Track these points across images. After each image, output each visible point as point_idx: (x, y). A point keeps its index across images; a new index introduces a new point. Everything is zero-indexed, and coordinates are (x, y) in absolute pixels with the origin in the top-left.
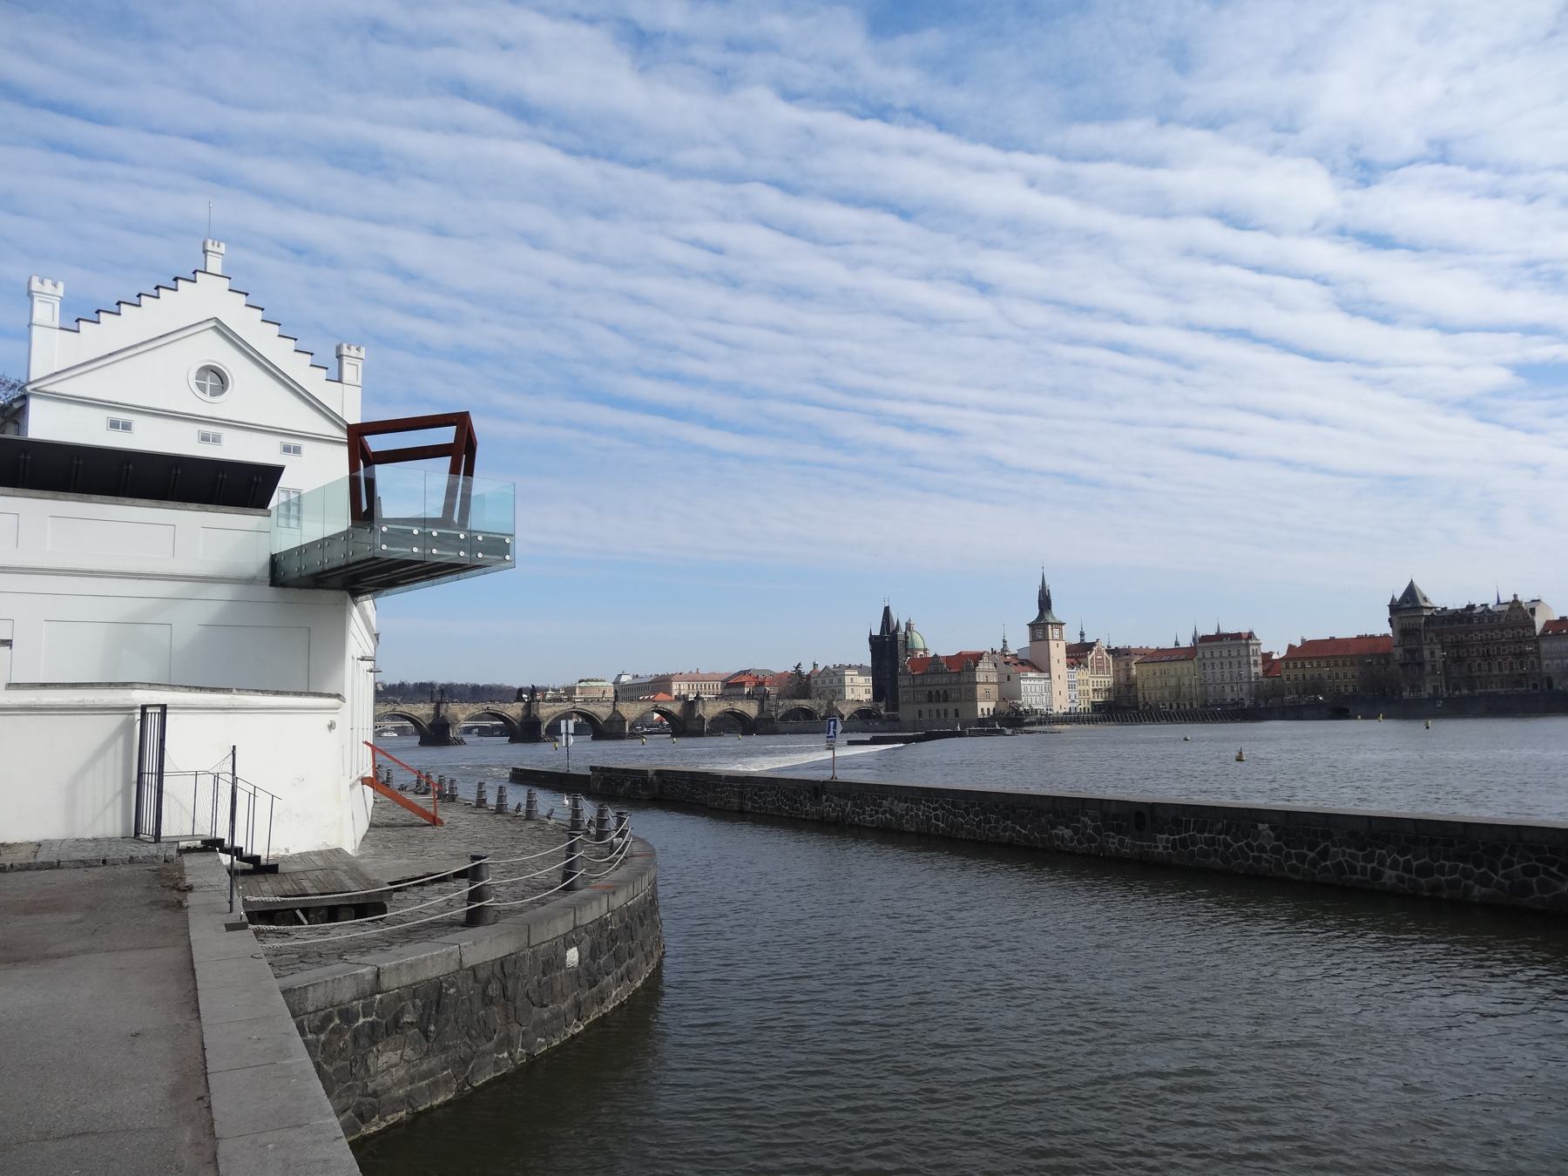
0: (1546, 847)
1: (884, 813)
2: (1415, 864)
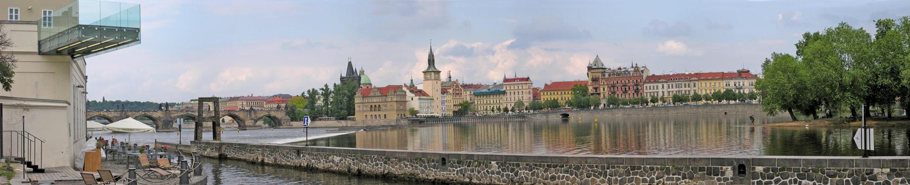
0: (595, 165)
1: (330, 162)
2: (550, 176)
